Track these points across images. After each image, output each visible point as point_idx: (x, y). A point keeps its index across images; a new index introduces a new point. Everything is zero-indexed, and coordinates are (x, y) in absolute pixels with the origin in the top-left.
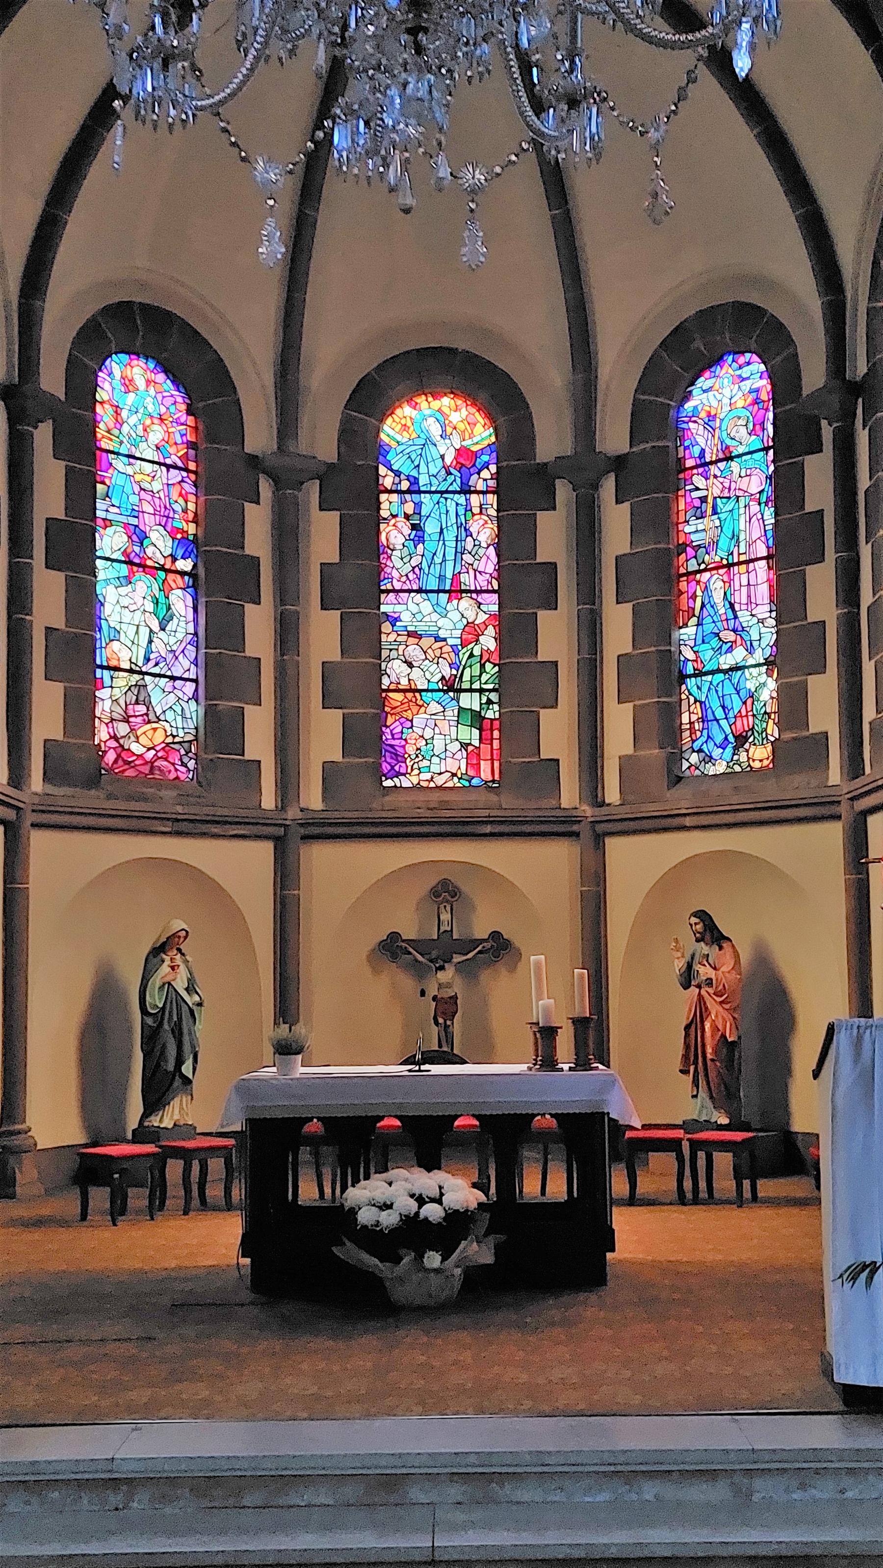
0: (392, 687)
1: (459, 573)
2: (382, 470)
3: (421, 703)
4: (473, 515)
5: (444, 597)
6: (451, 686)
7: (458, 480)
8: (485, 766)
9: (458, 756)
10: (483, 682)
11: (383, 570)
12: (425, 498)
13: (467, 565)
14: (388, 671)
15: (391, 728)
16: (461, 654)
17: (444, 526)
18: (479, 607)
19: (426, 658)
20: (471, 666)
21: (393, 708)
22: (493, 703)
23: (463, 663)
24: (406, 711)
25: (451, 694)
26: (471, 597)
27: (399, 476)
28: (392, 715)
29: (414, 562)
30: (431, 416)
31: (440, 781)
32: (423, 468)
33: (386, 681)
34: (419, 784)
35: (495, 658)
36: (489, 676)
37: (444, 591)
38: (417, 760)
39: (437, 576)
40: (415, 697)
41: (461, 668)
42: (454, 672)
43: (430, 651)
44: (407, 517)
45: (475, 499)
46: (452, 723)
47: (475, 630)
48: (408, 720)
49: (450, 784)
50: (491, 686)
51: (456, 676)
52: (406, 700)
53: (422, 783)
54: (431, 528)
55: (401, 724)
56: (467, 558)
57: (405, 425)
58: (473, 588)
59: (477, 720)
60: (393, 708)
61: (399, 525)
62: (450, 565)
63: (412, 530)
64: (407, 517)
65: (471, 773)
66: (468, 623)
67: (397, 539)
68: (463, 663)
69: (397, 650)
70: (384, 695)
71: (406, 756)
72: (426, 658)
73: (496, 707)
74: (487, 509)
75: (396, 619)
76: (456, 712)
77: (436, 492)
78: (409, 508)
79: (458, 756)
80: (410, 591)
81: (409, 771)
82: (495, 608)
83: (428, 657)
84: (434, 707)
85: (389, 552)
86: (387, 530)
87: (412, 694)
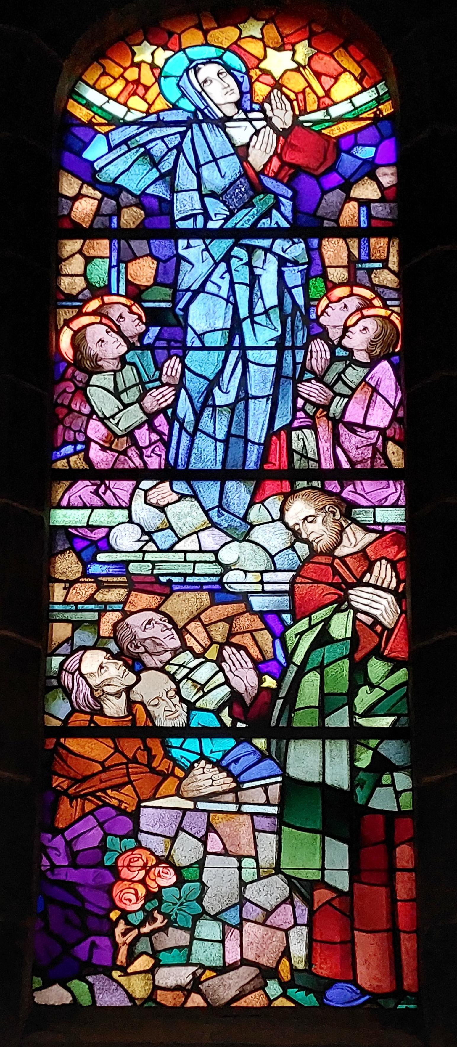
0: (80, 720)
1: (289, 428)
2: (69, 185)
3: (165, 766)
4: (330, 286)
5: (238, 494)
6: (259, 720)
7: (287, 207)
8: (367, 947)
9: (284, 916)
10: (360, 709)
11: (61, 422)
12: (193, 250)
13: (310, 409)
14: (67, 679)
15: (69, 835)
16: (290, 634)
17: (244, 312)
18: (347, 515)
19: (185, 647)
20: (321, 668)
21: (75, 781)
22: (392, 768)
23: (298, 658)
24: (118, 787)
25: (261, 743)
26: (323, 491)
27: (116, 198)
28: (72, 798)
29: (157, 398)
30: (209, 61)
31: (225, 988)
32: (186, 178)
33: (60, 708)
34: (152, 997)
35: (397, 646)
36: (379, 693)
37: (241, 475)
38: (146, 929)
39: (221, 435)
40: (148, 749)
41: (293, 670)
42: (270, 682)
43: (195, 628)
44: (135, 293)
45: (335, 251)
46: (262, 823)
47: (336, 572)
48: (123, 812)
49: (254, 1000)
50: (386, 722)
51: (274, 693)
52: (118, 758)
53: (161, 997)
54: (207, 316)
55: (101, 825)
56: (312, 390)
57: (137, 82)
58: (327, 464)
59: (335, 812)
60: (75, 781)
61: (114, 313)
62: (259, 412)
63: (148, 325)
64: (135, 293)
65: (323, 969)
66: (313, 552)
67: (105, 345)
68: (298, 658)
69: (97, 624)
70: (50, 743)
71: (114, 915)
72: (185, 647)
73: (403, 781)
74: (370, 271)
75: (93, 543)
76: (274, 791)
77: (221, 233)
78: (143, 271)
79: (284, 916)
80: (137, 475)
81: (122, 957)
82: (395, 516)
83: (191, 642)
84: (206, 779)
85: (80, 376)
86: (76, 325)
87: (138, 743)
